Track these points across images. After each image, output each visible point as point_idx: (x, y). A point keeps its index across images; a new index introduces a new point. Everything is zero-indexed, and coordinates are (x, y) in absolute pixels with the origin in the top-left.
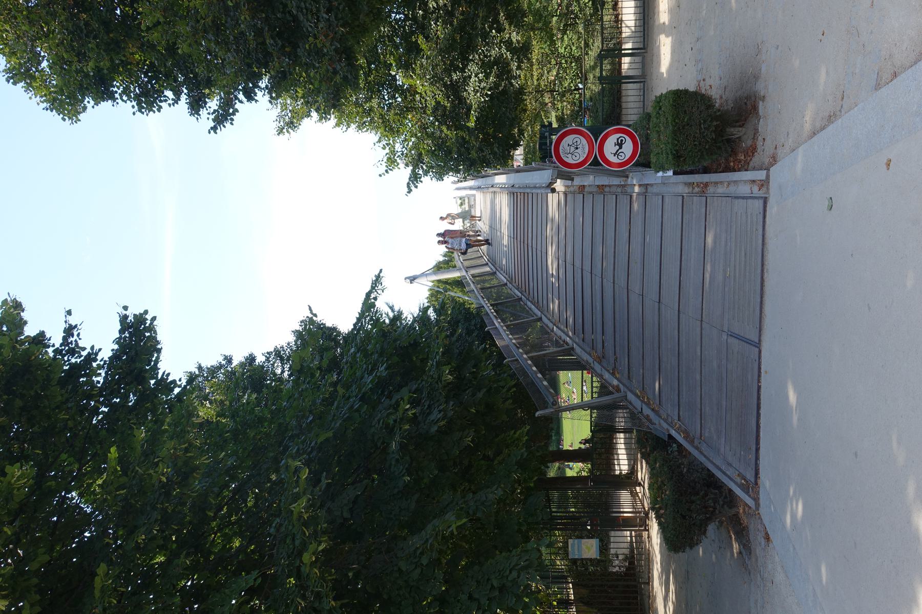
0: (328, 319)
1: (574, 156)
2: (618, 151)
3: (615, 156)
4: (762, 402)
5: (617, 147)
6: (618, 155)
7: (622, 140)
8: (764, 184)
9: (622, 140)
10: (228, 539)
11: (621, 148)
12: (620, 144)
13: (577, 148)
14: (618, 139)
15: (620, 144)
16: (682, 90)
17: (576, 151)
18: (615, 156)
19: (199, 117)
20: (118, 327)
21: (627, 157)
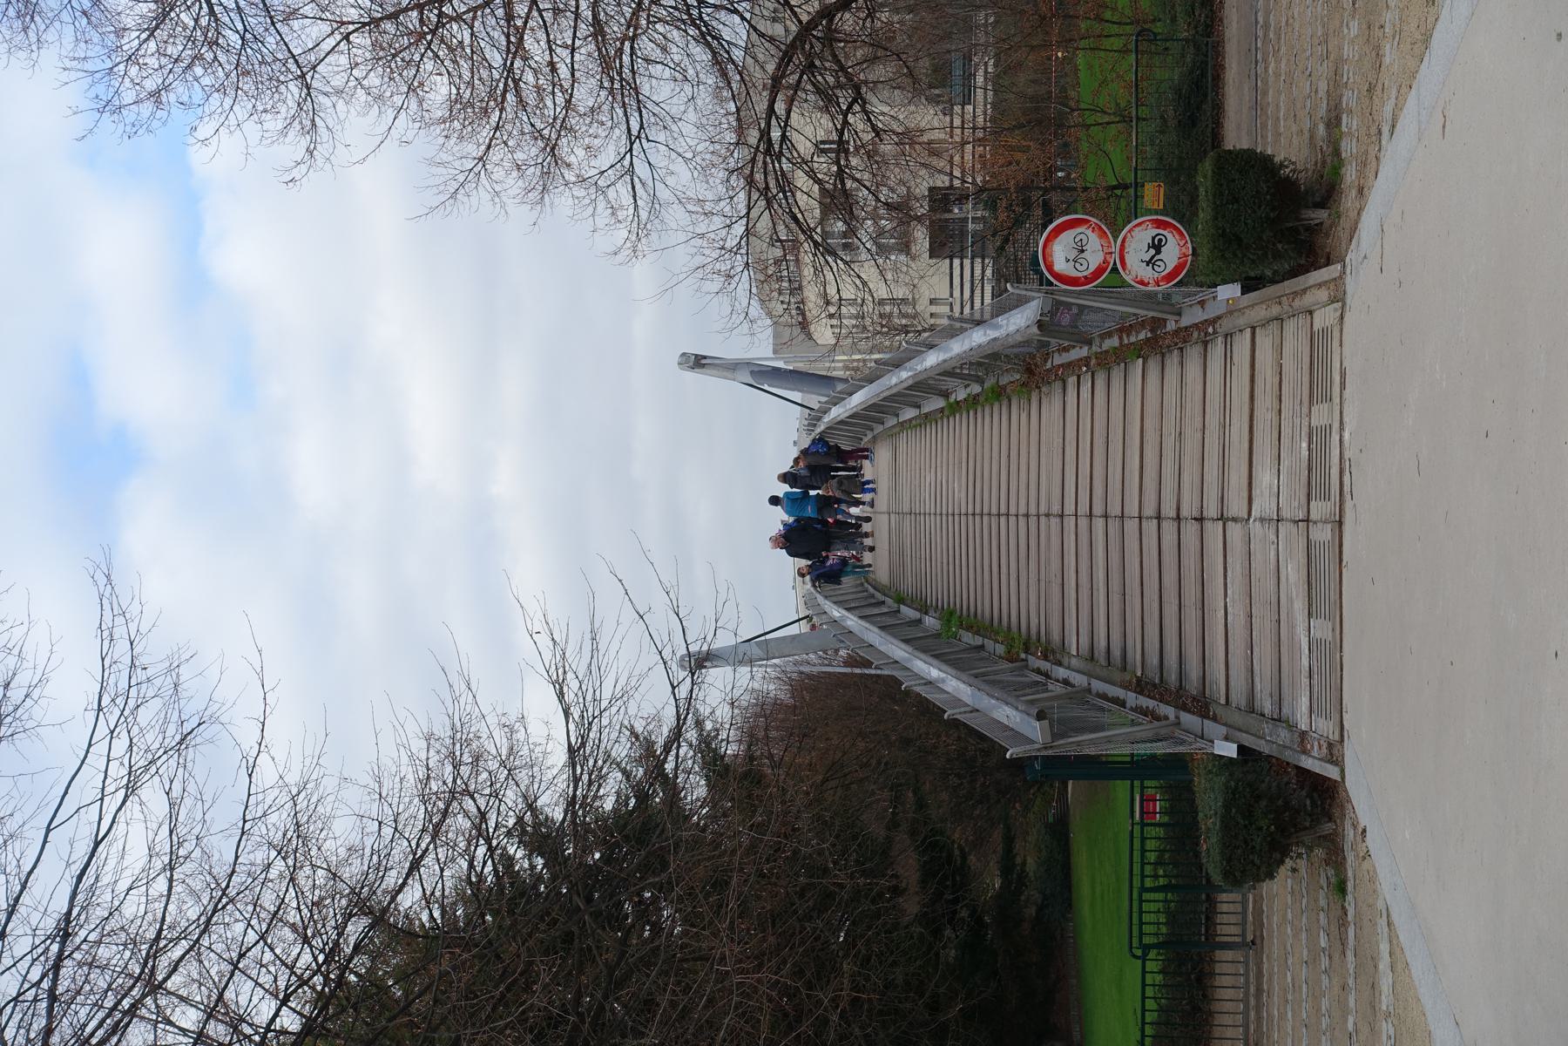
0: (777, 528)
1: (1077, 265)
2: (1153, 257)
3: (1148, 265)
4: (1257, 361)
5: (1152, 252)
6: (1154, 264)
7: (1160, 240)
8: (1339, 281)
9: (1160, 240)
10: (587, 850)
11: (1158, 252)
12: (1157, 246)
13: (1083, 251)
14: (1153, 238)
15: (1157, 246)
16: (1278, 867)
17: (1083, 255)
18: (1148, 265)
19: (626, 252)
20: (1350, 284)
21: (1169, 269)
